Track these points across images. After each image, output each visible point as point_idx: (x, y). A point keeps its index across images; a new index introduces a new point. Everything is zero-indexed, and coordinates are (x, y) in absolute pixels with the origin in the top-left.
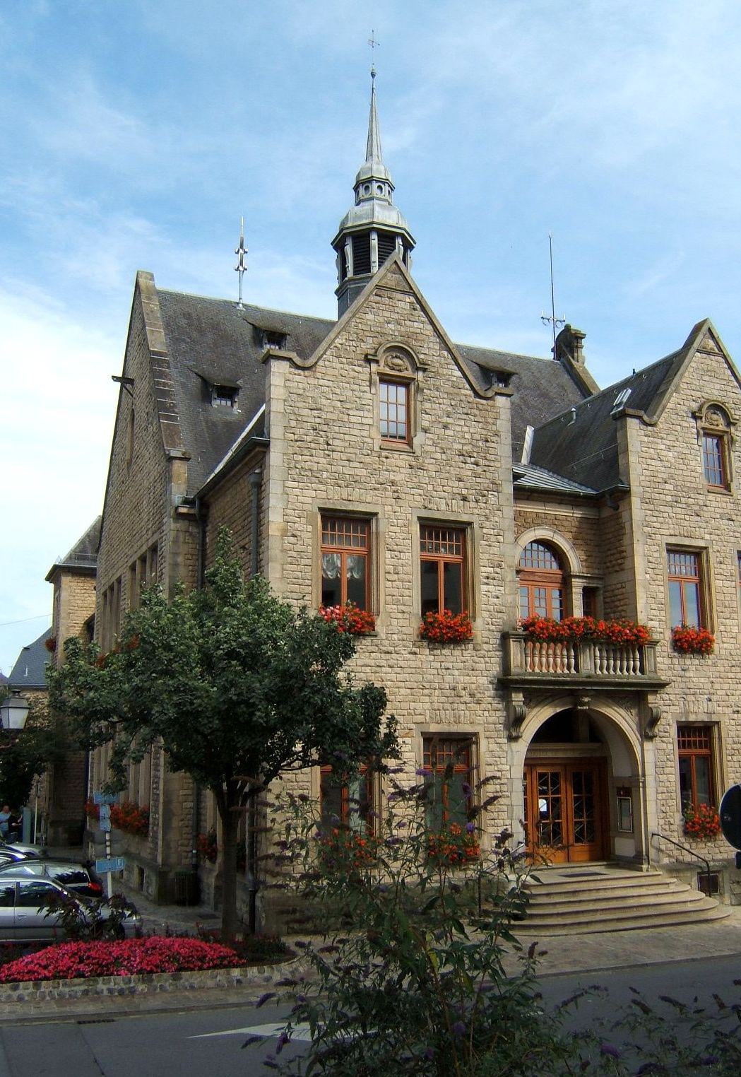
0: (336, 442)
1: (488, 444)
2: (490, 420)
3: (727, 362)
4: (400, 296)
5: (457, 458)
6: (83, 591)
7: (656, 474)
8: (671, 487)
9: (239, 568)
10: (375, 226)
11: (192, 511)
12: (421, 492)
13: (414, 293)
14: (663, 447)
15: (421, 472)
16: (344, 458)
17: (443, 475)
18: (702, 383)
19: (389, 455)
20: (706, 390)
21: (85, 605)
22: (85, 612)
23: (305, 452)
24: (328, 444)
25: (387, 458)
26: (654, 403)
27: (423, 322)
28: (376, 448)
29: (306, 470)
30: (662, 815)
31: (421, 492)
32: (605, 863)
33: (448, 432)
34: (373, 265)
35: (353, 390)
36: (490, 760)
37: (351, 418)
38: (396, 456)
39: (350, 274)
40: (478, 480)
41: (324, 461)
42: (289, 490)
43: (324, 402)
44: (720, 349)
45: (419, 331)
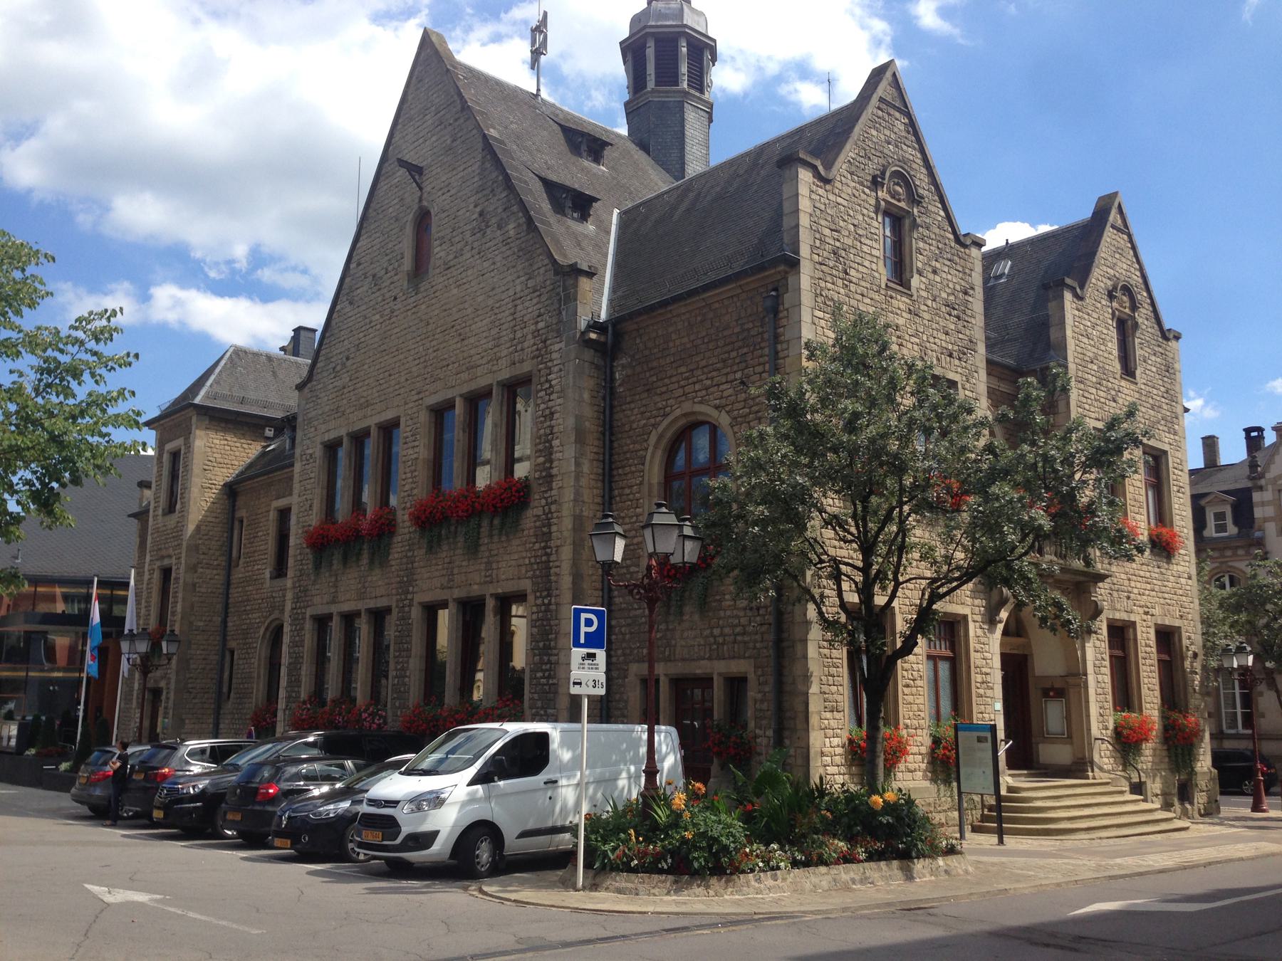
0: (853, 272)
1: (967, 297)
2: (967, 271)
3: (1131, 241)
4: (897, 115)
5: (943, 309)
6: (223, 442)
7: (1085, 352)
8: (1095, 368)
9: (94, 459)
10: (648, 30)
11: (602, 339)
12: (918, 341)
13: (909, 113)
14: (1089, 324)
15: (917, 320)
16: (859, 291)
17: (934, 326)
18: (1115, 261)
19: (894, 295)
20: (1118, 269)
21: (226, 461)
22: (225, 470)
23: (829, 279)
24: (847, 274)
25: (892, 298)
26: (788, 299)
27: (915, 149)
28: (883, 286)
29: (829, 300)
30: (1101, 719)
31: (918, 341)
32: (1025, 772)
33: (938, 279)
34: (648, 78)
35: (863, 215)
36: (978, 647)
37: (864, 247)
38: (899, 297)
39: (651, 84)
40: (960, 336)
41: (842, 291)
42: (816, 321)
43: (842, 223)
44: (1126, 226)
45: (911, 158)
